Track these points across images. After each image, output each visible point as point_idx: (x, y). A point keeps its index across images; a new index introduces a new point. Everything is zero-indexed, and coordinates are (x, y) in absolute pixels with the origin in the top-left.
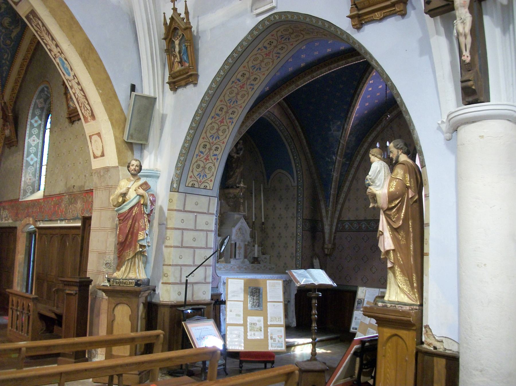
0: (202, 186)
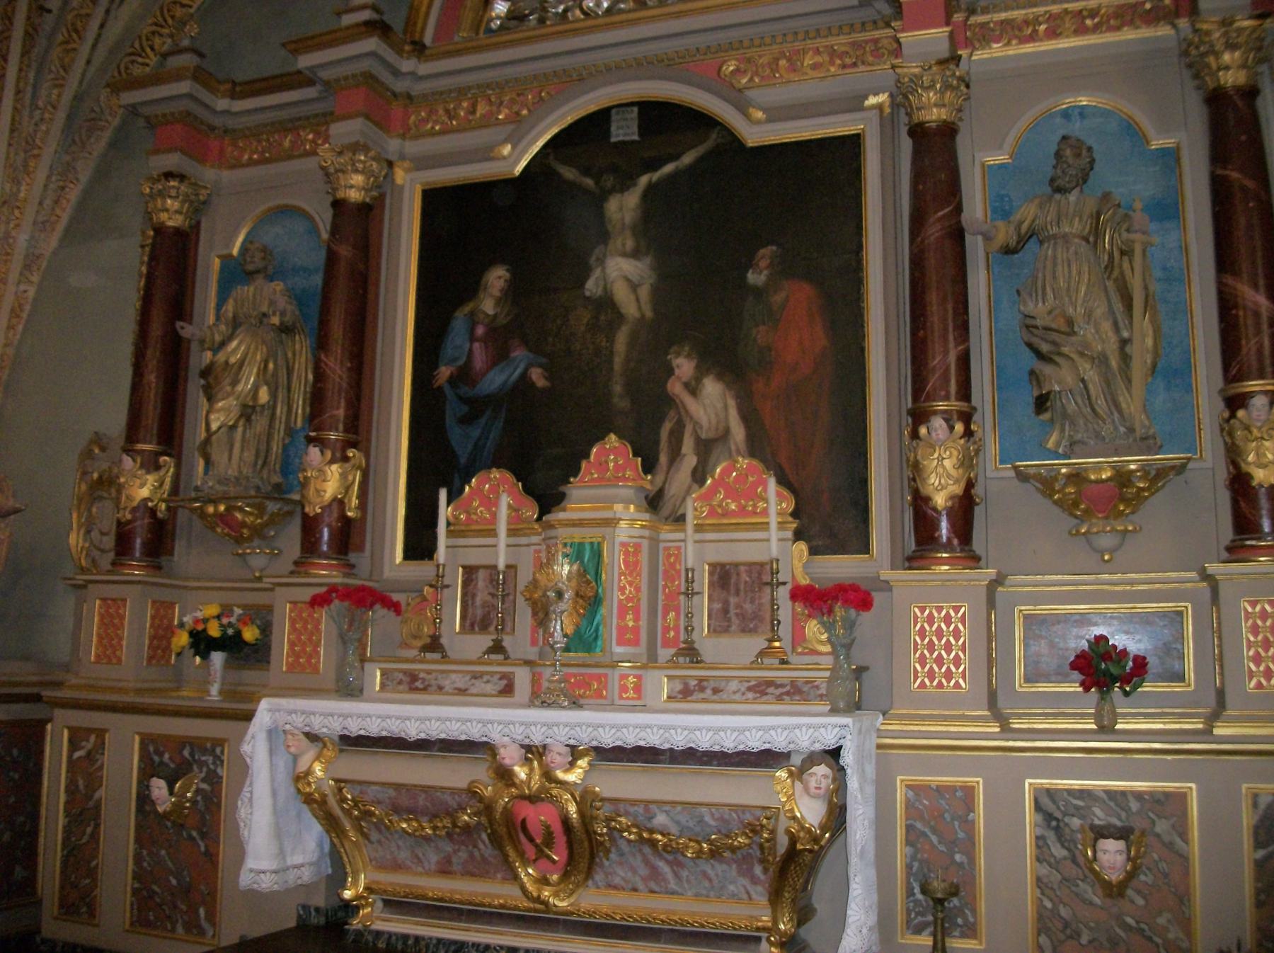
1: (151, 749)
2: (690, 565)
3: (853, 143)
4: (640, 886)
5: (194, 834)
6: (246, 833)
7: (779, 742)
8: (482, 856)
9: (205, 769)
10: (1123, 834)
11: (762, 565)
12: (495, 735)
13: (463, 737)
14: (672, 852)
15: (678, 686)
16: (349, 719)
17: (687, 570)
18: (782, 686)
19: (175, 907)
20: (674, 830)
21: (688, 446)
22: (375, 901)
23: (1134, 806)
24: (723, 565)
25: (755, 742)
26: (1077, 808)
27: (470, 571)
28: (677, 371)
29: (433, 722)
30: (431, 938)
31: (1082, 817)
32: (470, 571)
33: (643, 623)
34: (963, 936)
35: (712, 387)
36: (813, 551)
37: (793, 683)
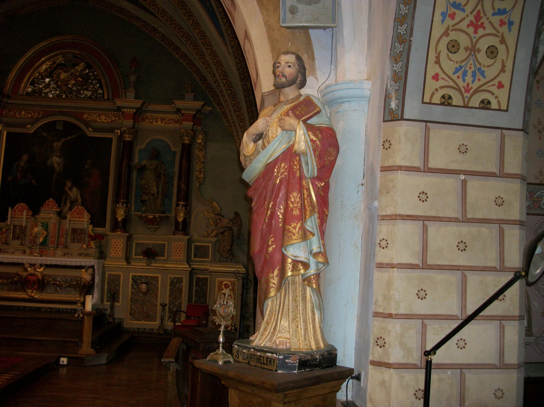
0: (476, 101)
2: (67, 228)
3: (110, 140)
4: (53, 293)
7: (83, 264)
10: (147, 283)
11: (83, 229)
12: (25, 262)
13: (17, 262)
14: (60, 286)
17: (66, 229)
18: (85, 254)
21: (68, 202)
23: (150, 279)
24: (74, 229)
25: (78, 264)
26: (139, 279)
27: (15, 226)
28: (67, 185)
31: (140, 280)
32: (15, 226)
33: (56, 240)
34: (117, 302)
35: (75, 190)
36: (94, 227)
37: (87, 254)
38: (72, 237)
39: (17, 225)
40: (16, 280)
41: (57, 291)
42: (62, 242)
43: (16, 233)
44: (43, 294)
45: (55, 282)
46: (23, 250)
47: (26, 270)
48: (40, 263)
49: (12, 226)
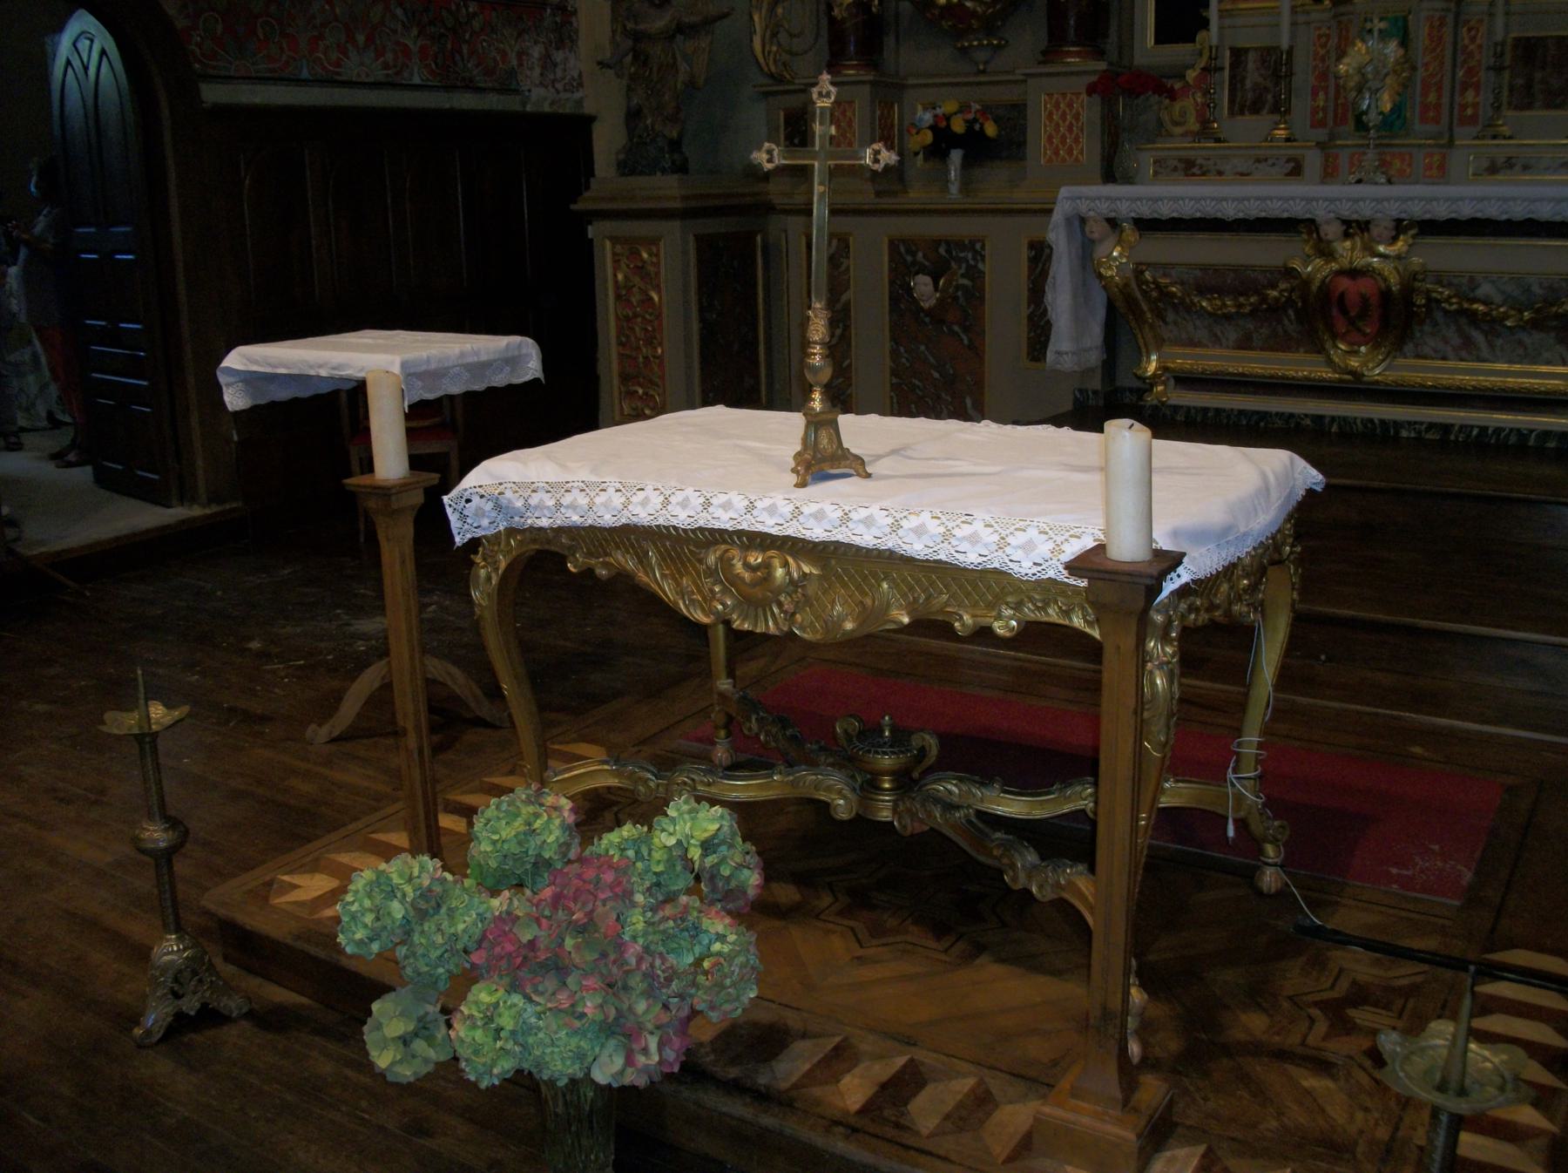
1: (902, 249)
5: (956, 328)
6: (1054, 317)
8: (1285, 331)
9: (964, 265)
12: (1320, 212)
13: (1285, 215)
15: (1486, 164)
16: (1160, 203)
19: (939, 397)
20: (1498, 299)
22: (1168, 379)
27: (1238, 54)
29: (1252, 201)
30: (1232, 410)
32: (1238, 54)
33: (1445, 100)
38: (1520, 81)
39: (1246, 50)
40: (1277, 300)
41: (1468, 343)
42: (1469, 112)
43: (1248, 84)
44: (1400, 361)
45: (1466, 305)
46: (1288, 161)
47: (1326, 252)
48: (1395, 214)
49: (1228, 53)
